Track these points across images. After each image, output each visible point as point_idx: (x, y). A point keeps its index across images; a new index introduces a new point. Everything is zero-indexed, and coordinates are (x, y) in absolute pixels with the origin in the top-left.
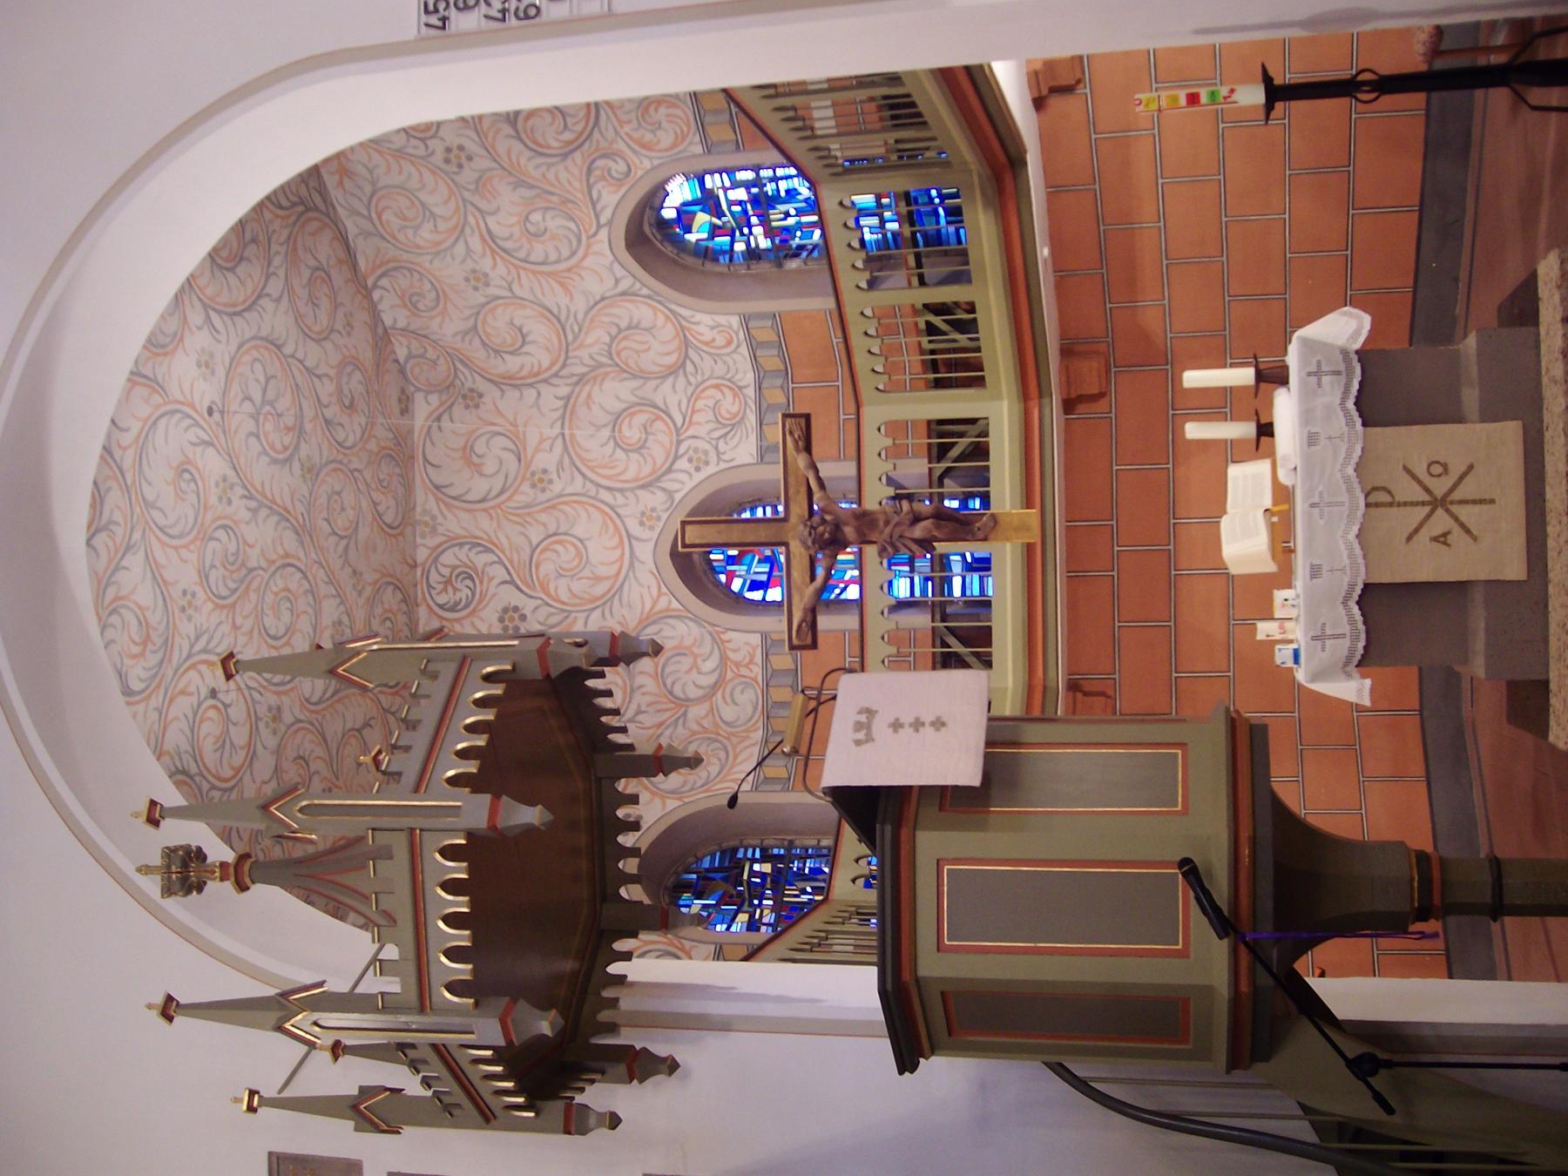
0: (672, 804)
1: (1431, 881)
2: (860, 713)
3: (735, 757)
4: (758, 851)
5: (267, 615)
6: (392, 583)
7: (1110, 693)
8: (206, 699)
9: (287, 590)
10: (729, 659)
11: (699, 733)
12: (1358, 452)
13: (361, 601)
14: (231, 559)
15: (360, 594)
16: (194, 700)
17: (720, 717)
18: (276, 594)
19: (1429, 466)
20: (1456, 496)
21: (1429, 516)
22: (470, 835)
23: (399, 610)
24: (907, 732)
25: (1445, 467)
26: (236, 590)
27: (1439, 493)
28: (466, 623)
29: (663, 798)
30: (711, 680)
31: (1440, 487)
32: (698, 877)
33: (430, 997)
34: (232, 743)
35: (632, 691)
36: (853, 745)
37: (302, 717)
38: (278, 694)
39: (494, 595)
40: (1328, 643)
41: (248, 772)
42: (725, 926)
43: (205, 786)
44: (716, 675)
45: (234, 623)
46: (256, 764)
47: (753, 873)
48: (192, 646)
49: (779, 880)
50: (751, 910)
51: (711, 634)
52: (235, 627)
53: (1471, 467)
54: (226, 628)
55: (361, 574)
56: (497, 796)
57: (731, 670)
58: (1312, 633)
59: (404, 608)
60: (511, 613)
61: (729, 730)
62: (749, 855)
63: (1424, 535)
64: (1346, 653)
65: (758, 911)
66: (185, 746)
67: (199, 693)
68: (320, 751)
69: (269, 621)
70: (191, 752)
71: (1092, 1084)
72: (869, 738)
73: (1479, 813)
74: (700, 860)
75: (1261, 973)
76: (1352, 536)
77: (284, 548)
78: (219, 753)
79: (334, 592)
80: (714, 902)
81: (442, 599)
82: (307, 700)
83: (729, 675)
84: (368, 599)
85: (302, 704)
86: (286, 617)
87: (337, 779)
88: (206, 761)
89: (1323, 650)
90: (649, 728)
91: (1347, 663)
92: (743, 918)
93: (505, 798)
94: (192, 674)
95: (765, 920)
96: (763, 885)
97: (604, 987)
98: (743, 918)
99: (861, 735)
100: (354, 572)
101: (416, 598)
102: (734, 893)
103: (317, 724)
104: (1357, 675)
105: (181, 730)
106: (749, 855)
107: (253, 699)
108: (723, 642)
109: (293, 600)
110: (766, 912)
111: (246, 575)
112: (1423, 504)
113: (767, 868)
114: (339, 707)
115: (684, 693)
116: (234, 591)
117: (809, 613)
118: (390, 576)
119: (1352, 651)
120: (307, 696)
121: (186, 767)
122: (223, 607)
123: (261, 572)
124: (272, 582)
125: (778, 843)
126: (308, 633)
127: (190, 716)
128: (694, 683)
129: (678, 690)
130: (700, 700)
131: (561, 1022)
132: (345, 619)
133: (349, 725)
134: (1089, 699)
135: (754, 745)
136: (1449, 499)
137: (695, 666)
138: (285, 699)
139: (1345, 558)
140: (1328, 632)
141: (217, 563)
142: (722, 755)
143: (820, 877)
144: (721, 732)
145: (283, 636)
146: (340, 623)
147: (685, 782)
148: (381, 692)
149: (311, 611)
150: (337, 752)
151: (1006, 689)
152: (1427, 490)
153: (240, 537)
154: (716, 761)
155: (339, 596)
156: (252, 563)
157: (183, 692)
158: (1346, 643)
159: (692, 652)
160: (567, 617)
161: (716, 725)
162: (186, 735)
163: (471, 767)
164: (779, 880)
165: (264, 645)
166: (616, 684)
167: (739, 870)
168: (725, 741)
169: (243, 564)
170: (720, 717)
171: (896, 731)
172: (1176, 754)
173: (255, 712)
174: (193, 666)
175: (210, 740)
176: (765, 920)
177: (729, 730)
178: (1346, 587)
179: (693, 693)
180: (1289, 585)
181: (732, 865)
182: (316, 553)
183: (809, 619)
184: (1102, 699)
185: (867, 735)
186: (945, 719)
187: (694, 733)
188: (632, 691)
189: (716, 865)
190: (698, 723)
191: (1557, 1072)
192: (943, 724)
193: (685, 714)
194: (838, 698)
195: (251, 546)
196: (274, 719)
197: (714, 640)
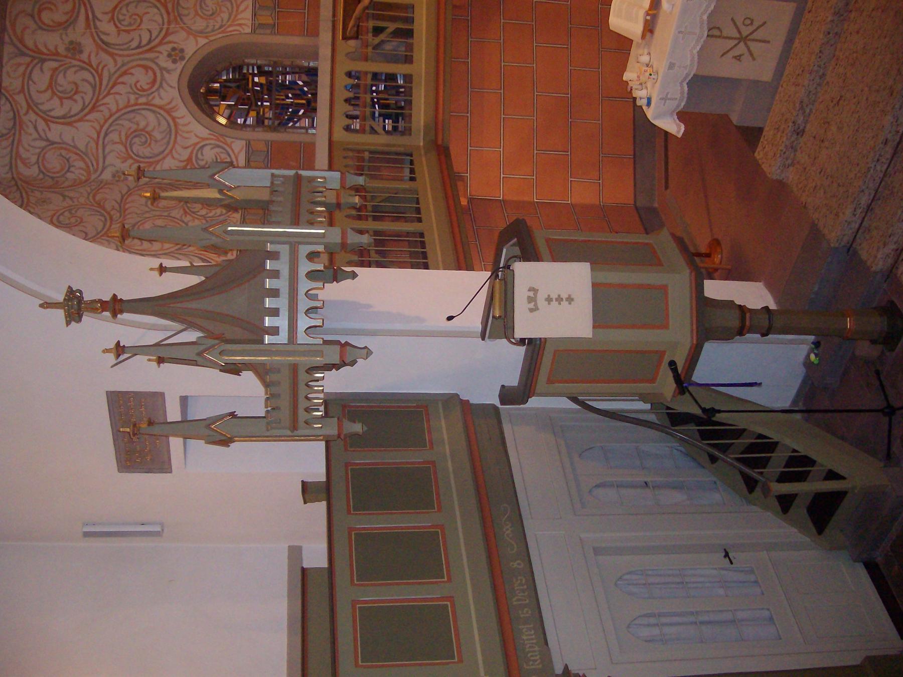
0: (202, 41)
2: (529, 291)
3: (238, 7)
4: (255, 68)
12: (712, 7)
19: (745, 19)
20: (754, 36)
21: (736, 45)
25: (752, 21)
27: (744, 34)
29: (195, 37)
31: (745, 31)
40: (667, 101)
42: (243, 120)
47: (256, 84)
53: (765, 23)
58: (661, 97)
63: (731, 54)
76: (695, 52)
80: (233, 103)
92: (253, 114)
98: (253, 114)
99: (532, 306)
102: (245, 97)
110: (267, 110)
112: (735, 39)
113: (263, 80)
136: (748, 38)
139: (689, 61)
140: (669, 96)
143: (296, 87)
147: (208, 26)
152: (740, 32)
154: (224, 9)
158: (676, 102)
167: (246, 81)
176: (267, 115)
181: (241, 77)
185: (534, 306)
191: (780, 414)
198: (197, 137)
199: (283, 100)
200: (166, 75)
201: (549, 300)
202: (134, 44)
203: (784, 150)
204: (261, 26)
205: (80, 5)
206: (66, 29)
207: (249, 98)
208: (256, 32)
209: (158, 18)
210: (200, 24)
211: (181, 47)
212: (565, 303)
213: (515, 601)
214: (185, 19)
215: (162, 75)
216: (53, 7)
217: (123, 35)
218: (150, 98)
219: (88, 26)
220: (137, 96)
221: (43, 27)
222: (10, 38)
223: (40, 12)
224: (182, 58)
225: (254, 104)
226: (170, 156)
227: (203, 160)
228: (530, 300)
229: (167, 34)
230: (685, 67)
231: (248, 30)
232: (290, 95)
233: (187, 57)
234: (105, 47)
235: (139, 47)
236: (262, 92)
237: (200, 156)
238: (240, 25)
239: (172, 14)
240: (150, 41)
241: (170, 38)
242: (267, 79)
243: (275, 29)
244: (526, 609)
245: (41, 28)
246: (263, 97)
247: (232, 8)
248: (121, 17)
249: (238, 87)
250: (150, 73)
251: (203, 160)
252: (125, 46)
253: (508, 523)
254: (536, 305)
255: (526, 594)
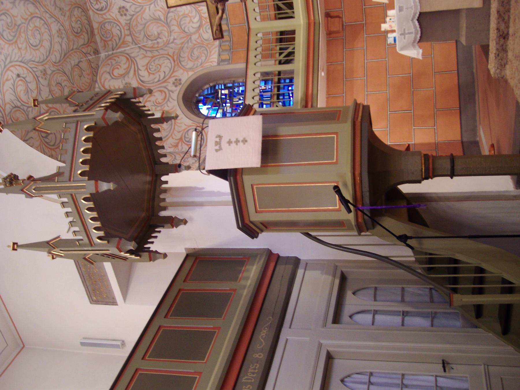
0: (191, 73)
1: (429, 168)
2: (216, 137)
3: (210, 52)
5: (31, 39)
6: (76, 7)
7: (341, 16)
8: (16, 78)
9: (36, 27)
10: (203, 17)
11: (197, 44)
13: (66, 18)
14: (10, 25)
15: (64, 16)
16: (12, 81)
17: (203, 38)
18: (32, 30)
22: (91, 194)
23: (82, 15)
24: (233, 145)
26: (16, 35)
28: (107, 14)
29: (187, 71)
30: (196, 25)
32: (204, 98)
33: (93, 242)
34: (30, 89)
35: (171, 32)
36: (215, 151)
37: (55, 69)
38: (43, 65)
39: (115, 3)
40: (406, 36)
41: (40, 97)
43: (25, 108)
44: (199, 23)
45: (18, 47)
46: (42, 93)
47: (222, 94)
48: (5, 63)
49: (232, 95)
50: (223, 108)
51: (194, 8)
52: (19, 49)
54: (16, 50)
55: (63, 9)
56: (96, 181)
57: (204, 20)
58: (400, 33)
59: (83, 14)
60: (122, 9)
61: (207, 42)
62: (220, 88)
64: (413, 39)
65: (225, 108)
66: (13, 98)
67: (13, 78)
68: (65, 78)
69: (32, 41)
70: (16, 99)
71: (317, 237)
72: (220, 149)
73: (474, 55)
74: (203, 91)
75: (366, 217)
77: (29, 11)
78: (27, 96)
79: (54, 20)
81: (97, 7)
82: (55, 63)
83: (204, 22)
84: (69, 16)
85: (53, 65)
86: (38, 37)
87: (73, 84)
88: (22, 98)
89: (405, 38)
90: (179, 45)
91: (414, 42)
92: (220, 111)
93: (99, 182)
94: (9, 73)
95: (228, 111)
96: (226, 98)
97: (160, 194)
98: (220, 111)
99: (217, 147)
100: (60, 9)
101: (87, 8)
102: (216, 102)
103: (61, 69)
104: (417, 47)
105: (11, 94)
106: (220, 88)
107: (34, 71)
108: (199, 11)
109: (39, 29)
111: (18, 28)
113: (226, 92)
114: (68, 60)
115: (189, 30)
116: (14, 37)
117: (218, 26)
118: (75, 4)
119: (415, 38)
120: (54, 61)
121: (16, 105)
122: (12, 44)
123: (23, 25)
124: (29, 26)
125: (229, 82)
126: (49, 39)
127: (12, 87)
128: (192, 27)
129: (186, 30)
130: (194, 33)
131: (136, 245)
132: (61, 28)
133: (73, 65)
134: (333, 19)
135: (216, 47)
137: (191, 20)
138: (47, 66)
140: (406, 32)
141: (5, 28)
142: (206, 52)
144: (204, 43)
145: (39, 44)
146: (60, 30)
147: (194, 65)
148: (83, 48)
149: (47, 31)
150: (71, 75)
151: (300, 25)
153: (10, 15)
154: (203, 55)
155: (57, 20)
156: (19, 23)
157: (7, 80)
159: (189, 16)
160: (142, 8)
161: (202, 41)
162: (13, 94)
163: (87, 168)
164: (232, 95)
165: (32, 50)
166: (165, 30)
168: (206, 46)
169: (15, 25)
170: (203, 38)
171: (230, 145)
172: (334, 137)
173: (36, 75)
174: (8, 69)
175: (22, 92)
176: (228, 111)
177: (207, 42)
178: (412, 14)
179: (192, 30)
180: (393, 8)
182: (43, 8)
183: (219, 28)
184: (338, 19)
185: (219, 147)
186: (247, 139)
187: (195, 45)
188: (171, 32)
189: (209, 92)
190: (196, 41)
192: (246, 141)
193: (191, 38)
194: (209, 126)
195: (16, 17)
196: (44, 75)
197: (196, 10)
198: (185, 125)
199: (238, 101)
200: (171, 93)
201: (230, 142)
202: (156, 80)
203: (497, 54)
204: (223, 61)
205: (132, 63)
206: (124, 77)
207: (219, 102)
208: (220, 64)
209: (169, 65)
210: (190, 65)
211: (179, 78)
212: (241, 144)
213: (244, 380)
214: (183, 63)
215: (169, 94)
216: (119, 67)
217: (151, 75)
218: (163, 106)
219: (135, 74)
220: (156, 107)
221: (114, 77)
222: (99, 86)
223: (113, 70)
224: (180, 84)
225: (221, 106)
226: (171, 137)
227: (188, 138)
228: (217, 143)
229: (173, 72)
230: (411, 8)
231: (215, 64)
232: (242, 98)
233: (182, 83)
234: (142, 83)
235: (159, 81)
236: (226, 98)
237: (187, 136)
238: (211, 62)
239: (176, 62)
240: (164, 77)
241: (174, 74)
242: (229, 91)
243: (229, 61)
244: (249, 386)
245: (113, 78)
246: (226, 101)
247: (207, 53)
248: (151, 67)
249: (213, 97)
250: (164, 94)
251: (188, 138)
252: (151, 82)
253: (266, 328)
254: (220, 147)
255: (255, 375)
